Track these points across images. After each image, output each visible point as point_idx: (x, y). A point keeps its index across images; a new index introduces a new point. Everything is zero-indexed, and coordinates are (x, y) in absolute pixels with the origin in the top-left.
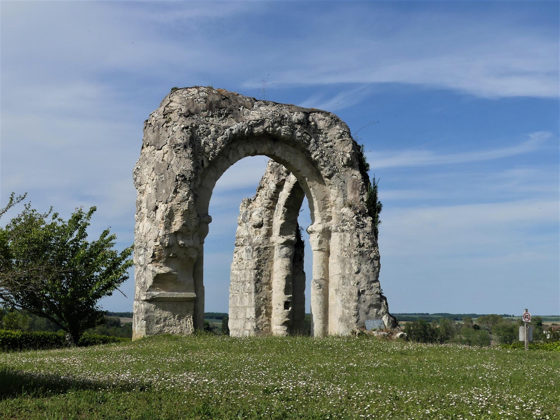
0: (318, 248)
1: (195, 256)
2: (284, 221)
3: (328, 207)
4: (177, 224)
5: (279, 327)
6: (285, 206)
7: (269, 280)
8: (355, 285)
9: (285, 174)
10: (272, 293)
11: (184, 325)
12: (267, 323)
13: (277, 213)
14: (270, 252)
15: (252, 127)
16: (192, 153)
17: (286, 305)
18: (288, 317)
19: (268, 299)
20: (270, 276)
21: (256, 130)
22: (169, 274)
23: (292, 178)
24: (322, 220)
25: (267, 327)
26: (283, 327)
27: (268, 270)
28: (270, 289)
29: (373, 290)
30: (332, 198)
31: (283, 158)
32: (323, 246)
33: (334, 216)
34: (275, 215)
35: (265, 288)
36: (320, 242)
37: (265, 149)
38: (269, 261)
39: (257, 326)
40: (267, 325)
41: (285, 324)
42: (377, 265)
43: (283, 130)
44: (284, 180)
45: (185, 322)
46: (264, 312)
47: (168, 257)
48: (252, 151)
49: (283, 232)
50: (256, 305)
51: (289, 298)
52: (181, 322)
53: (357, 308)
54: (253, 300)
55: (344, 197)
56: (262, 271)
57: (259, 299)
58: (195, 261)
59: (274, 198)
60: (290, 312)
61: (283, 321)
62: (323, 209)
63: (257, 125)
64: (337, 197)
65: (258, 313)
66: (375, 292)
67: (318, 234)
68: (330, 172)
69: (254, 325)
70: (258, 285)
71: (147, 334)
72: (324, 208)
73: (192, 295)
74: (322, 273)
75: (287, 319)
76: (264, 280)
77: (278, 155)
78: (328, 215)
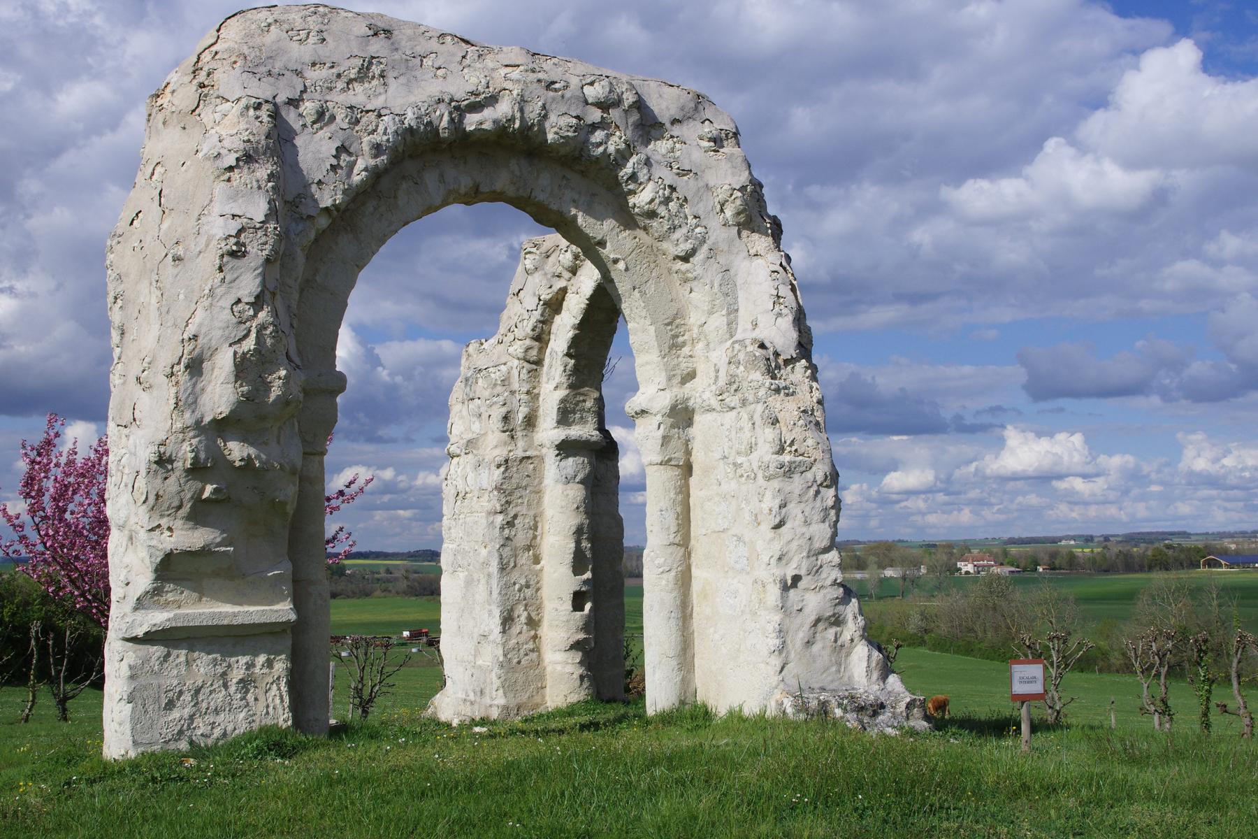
0: (658, 459)
1: (288, 492)
2: (567, 392)
3: (684, 344)
4: (220, 394)
5: (560, 656)
6: (568, 355)
7: (535, 537)
8: (773, 561)
9: (567, 275)
10: (541, 570)
11: (260, 708)
12: (531, 645)
13: (548, 374)
14: (534, 469)
15: (460, 111)
16: (271, 177)
17: (578, 600)
18: (585, 628)
19: (532, 585)
20: (536, 528)
21: (471, 122)
22: (205, 552)
23: (589, 278)
24: (669, 379)
25: (534, 656)
26: (573, 652)
27: (532, 513)
28: (537, 560)
29: (824, 575)
30: (694, 319)
31: (554, 207)
32: (585, 430)
33: (701, 369)
34: (544, 378)
35: (524, 559)
36: (666, 440)
37: (502, 181)
38: (531, 492)
39: (505, 655)
40: (533, 651)
41: (576, 646)
42: (830, 502)
43: (557, 127)
44: (564, 291)
45: (262, 698)
46: (523, 619)
47: (198, 501)
48: (465, 183)
49: (565, 416)
50: (503, 603)
51: (586, 582)
52: (250, 697)
53: (781, 632)
54: (496, 592)
55: (729, 314)
56: (515, 517)
57: (507, 586)
58: (290, 509)
59: (541, 337)
60: (589, 616)
61: (571, 641)
62: (671, 348)
63: (475, 107)
64: (711, 313)
65: (507, 620)
66: (829, 582)
67: (659, 418)
68: (688, 246)
69: (500, 652)
70: (507, 552)
71: (135, 743)
72: (674, 346)
73: (283, 610)
74: (673, 528)
75: (581, 636)
76: (521, 538)
77: (541, 197)
78: (683, 365)
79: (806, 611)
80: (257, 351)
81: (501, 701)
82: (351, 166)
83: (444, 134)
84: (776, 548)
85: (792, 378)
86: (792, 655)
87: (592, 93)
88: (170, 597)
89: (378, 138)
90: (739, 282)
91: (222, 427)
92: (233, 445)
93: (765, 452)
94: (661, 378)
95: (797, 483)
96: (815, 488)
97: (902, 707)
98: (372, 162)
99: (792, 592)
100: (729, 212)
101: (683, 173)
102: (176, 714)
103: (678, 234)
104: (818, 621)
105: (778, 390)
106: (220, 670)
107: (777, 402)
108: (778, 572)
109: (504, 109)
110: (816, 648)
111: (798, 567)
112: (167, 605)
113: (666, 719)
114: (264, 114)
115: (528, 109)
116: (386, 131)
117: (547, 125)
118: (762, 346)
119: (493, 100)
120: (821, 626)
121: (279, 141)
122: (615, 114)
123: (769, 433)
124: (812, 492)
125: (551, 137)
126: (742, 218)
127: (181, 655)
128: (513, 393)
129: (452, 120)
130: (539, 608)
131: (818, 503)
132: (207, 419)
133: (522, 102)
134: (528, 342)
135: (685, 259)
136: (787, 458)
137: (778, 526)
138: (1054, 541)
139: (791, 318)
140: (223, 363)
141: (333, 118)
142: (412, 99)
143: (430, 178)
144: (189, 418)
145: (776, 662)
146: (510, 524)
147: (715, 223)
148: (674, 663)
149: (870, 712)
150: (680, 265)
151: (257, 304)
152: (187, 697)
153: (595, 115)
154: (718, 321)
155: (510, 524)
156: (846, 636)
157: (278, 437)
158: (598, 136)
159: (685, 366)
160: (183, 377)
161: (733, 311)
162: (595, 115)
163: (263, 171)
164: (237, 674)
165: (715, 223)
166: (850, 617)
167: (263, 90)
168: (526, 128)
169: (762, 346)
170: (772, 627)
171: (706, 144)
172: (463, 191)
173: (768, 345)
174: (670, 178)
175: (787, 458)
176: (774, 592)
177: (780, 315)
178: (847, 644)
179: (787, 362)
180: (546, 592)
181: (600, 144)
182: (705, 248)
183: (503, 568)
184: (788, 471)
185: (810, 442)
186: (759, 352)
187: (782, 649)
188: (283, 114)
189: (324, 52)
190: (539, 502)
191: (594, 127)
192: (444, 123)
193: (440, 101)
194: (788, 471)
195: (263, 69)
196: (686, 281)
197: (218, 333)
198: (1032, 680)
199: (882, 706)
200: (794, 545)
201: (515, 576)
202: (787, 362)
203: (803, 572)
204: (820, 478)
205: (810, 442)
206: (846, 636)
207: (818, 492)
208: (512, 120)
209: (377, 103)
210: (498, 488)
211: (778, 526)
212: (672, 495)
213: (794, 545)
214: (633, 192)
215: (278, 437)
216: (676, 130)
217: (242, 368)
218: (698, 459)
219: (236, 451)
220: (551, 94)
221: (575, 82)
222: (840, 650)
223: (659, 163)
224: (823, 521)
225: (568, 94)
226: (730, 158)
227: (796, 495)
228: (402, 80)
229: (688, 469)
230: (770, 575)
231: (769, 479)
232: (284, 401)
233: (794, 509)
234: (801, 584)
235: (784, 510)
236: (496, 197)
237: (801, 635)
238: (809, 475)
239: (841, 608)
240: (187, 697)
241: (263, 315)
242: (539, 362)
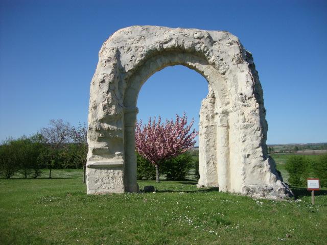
20: (215, 142)
21: (165, 46)
24: (222, 105)
25: (215, 172)
35: (212, 149)
37: (177, 59)
46: (212, 163)
47: (99, 138)
53: (244, 169)
63: (166, 43)
64: (231, 87)
68: (223, 71)
70: (208, 147)
73: (119, 160)
76: (211, 144)
79: (252, 164)
80: (108, 104)
81: (207, 182)
82: (135, 60)
83: (159, 50)
84: (243, 147)
85: (250, 102)
86: (247, 175)
87: (196, 36)
88: (96, 158)
89: (142, 53)
90: (238, 78)
91: (102, 121)
92: (105, 124)
93: (241, 123)
94: (220, 104)
95: (249, 130)
96: (254, 131)
97: (277, 190)
98: (141, 59)
99: (247, 159)
100: (234, 61)
101: (222, 53)
102: (98, 184)
103: (221, 68)
104: (255, 166)
105: (245, 106)
106: (107, 174)
107: (244, 109)
108: (244, 153)
109: (173, 42)
110: (254, 174)
111: (249, 152)
112: (95, 160)
113: (204, 190)
114: (114, 51)
115: (179, 42)
116: (144, 51)
117: (184, 45)
118: (242, 94)
119: (171, 40)
120: (256, 168)
121: (118, 55)
122: (202, 40)
123: (241, 117)
124: (253, 132)
125: (186, 47)
126: (238, 62)
127: (98, 171)
128: (209, 110)
129: (160, 47)
130: (216, 160)
131: (255, 135)
132: (99, 119)
133: (177, 40)
134: (211, 98)
135: (224, 74)
136: (246, 123)
137: (244, 141)
138: (297, 148)
139: (251, 87)
140: (101, 107)
141: (132, 50)
142: (151, 43)
143: (158, 61)
144: (95, 119)
145: (243, 177)
146: (208, 141)
147: (231, 64)
148: (224, 176)
149: (268, 191)
150: (223, 76)
151: (108, 92)
152: (100, 180)
153: (197, 41)
154: (233, 89)
155: (208, 141)
156: (264, 170)
157: (117, 123)
158: (198, 46)
159: (227, 101)
160: (93, 110)
161: (237, 86)
162: (197, 41)
163: (112, 63)
164: (111, 175)
165: (231, 64)
166: (265, 165)
167: (115, 46)
168: (179, 46)
169: (242, 94)
170: (242, 168)
171: (228, 44)
172: (167, 63)
173: (243, 94)
174: (218, 54)
175: (246, 123)
176: (242, 159)
177: (248, 86)
178: (264, 172)
179: (249, 98)
180: (217, 157)
181: (199, 48)
182: (229, 71)
183: (206, 152)
184: (246, 127)
185: (253, 119)
186: (240, 96)
187: (244, 174)
188: (120, 50)
189: (131, 35)
190: (216, 136)
191: (197, 44)
192: (158, 47)
193: (157, 42)
194: (246, 127)
195: (117, 41)
196: (225, 79)
197: (99, 100)
198: (315, 185)
199: (272, 189)
200: (248, 147)
201: (210, 153)
202: (249, 98)
203: (251, 154)
204: (256, 129)
205: (253, 119)
206: (264, 170)
207: (255, 132)
208: (175, 45)
209: (143, 45)
210: (205, 133)
211: (244, 141)
212: (224, 134)
213: (248, 147)
214: (209, 59)
215: (117, 123)
216: (220, 42)
217: (104, 108)
218: (230, 124)
219: (106, 126)
220: (185, 37)
221: (192, 34)
222: (262, 174)
223: (215, 51)
224: (257, 140)
225: (190, 37)
226: (234, 47)
227: (248, 133)
228: (149, 39)
229: (228, 127)
230: (242, 154)
231: (241, 129)
232: (115, 115)
233: (248, 137)
234: (250, 157)
235: (245, 138)
236: (177, 64)
237: (250, 170)
238: (253, 128)
239: (262, 163)
240: (100, 180)
241: (109, 95)
242: (214, 103)
